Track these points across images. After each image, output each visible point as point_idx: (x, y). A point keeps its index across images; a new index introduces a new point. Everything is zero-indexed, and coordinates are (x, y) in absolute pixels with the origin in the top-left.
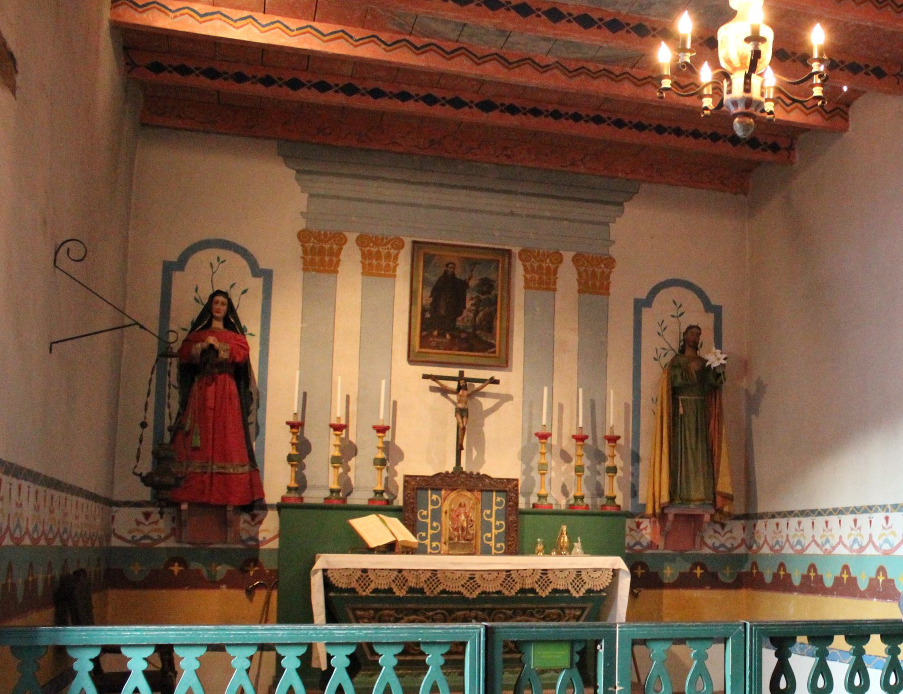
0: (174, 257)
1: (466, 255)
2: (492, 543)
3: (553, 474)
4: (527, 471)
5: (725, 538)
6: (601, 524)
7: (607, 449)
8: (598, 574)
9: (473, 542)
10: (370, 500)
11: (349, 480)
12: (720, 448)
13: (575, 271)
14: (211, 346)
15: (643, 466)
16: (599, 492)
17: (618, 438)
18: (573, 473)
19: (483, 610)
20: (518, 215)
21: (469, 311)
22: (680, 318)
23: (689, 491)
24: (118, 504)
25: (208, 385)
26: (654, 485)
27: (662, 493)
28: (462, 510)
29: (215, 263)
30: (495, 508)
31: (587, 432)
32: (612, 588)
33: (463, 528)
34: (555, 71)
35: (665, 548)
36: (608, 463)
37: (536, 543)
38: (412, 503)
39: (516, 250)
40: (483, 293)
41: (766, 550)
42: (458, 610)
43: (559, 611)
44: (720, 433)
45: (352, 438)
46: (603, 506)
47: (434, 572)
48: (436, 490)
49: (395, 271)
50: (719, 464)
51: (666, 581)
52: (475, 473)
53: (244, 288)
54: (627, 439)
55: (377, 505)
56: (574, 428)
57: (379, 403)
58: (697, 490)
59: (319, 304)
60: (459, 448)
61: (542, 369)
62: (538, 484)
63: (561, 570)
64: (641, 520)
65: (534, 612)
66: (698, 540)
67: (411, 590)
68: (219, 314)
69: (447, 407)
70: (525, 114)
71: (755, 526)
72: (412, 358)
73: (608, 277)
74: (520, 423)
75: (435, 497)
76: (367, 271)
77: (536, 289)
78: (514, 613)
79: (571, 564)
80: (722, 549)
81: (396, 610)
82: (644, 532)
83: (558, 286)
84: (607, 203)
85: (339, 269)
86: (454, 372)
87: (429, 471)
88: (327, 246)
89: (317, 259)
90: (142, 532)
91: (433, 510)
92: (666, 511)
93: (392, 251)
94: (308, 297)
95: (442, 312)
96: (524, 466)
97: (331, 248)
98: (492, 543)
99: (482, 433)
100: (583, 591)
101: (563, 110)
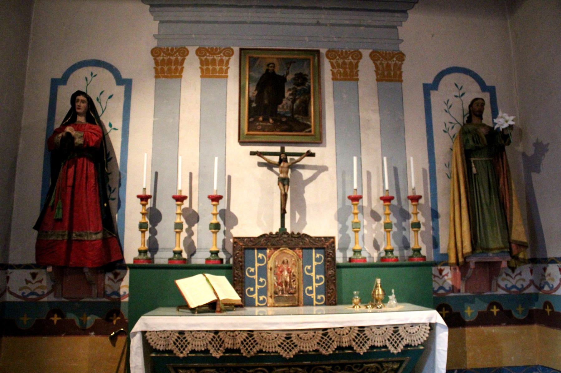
1: (282, 56)
2: (313, 296)
3: (366, 232)
4: (343, 230)
5: (515, 280)
6: (412, 277)
7: (410, 208)
8: (415, 329)
9: (296, 295)
10: (208, 260)
11: (193, 242)
12: (511, 201)
13: (373, 65)
14: (69, 134)
15: (441, 221)
16: (406, 246)
17: (420, 197)
18: (382, 230)
19: (302, 367)
20: (323, 25)
22: (462, 98)
24: (13, 267)
25: (69, 167)
26: (454, 235)
28: (285, 266)
29: (89, 78)
30: (315, 263)
31: (393, 194)
32: (429, 344)
33: (286, 282)
35: (466, 292)
36: (412, 220)
37: (353, 295)
38: (241, 262)
39: (323, 51)
40: (298, 85)
43: (377, 365)
44: (510, 189)
45: (195, 208)
46: (411, 258)
47: (250, 333)
48: (262, 249)
49: (226, 72)
50: (511, 215)
51: (467, 320)
52: (296, 233)
53: (111, 94)
55: (210, 264)
56: (381, 190)
58: (495, 240)
59: (167, 103)
60: (283, 212)
61: (351, 143)
63: (379, 327)
64: (442, 268)
67: (227, 350)
68: (86, 111)
71: (545, 269)
72: (241, 140)
73: (400, 68)
74: (335, 190)
75: (260, 255)
76: (205, 74)
80: (514, 290)
82: (446, 278)
84: (394, 11)
86: (277, 149)
87: (256, 232)
88: (173, 58)
89: (166, 68)
90: (29, 288)
91: (259, 268)
92: (467, 260)
93: (224, 58)
94: (158, 97)
95: (266, 102)
96: (340, 226)
97: (177, 59)
99: (303, 200)
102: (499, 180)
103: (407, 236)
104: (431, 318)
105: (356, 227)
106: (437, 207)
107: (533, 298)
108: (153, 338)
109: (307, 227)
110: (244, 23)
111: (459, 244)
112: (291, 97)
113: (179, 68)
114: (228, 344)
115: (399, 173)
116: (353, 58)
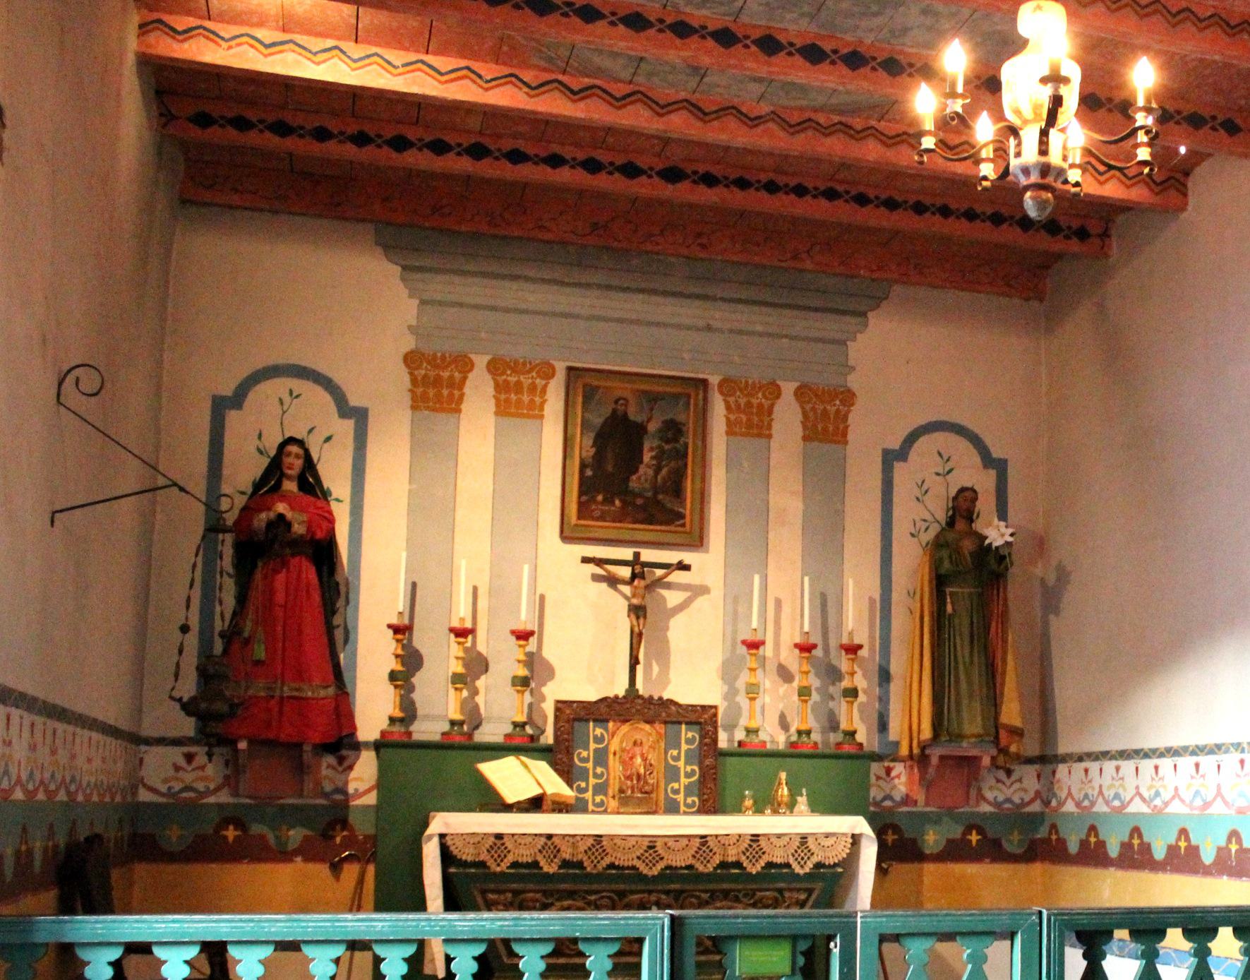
0: (227, 390)
2: (680, 797)
3: (767, 699)
4: (730, 695)
5: (1012, 790)
6: (836, 770)
7: (844, 664)
9: (654, 795)
10: (507, 736)
11: (477, 707)
12: (1004, 661)
13: (799, 410)
14: (281, 517)
15: (895, 687)
16: (833, 725)
18: (796, 697)
19: (667, 892)
21: (648, 466)
23: (960, 724)
24: (149, 742)
26: (911, 715)
27: (923, 726)
28: (637, 750)
29: (287, 399)
30: (684, 747)
31: (816, 638)
33: (639, 776)
34: (770, 125)
35: (927, 804)
36: (846, 683)
37: (743, 798)
38: (567, 740)
39: (714, 380)
40: (667, 442)
41: (1070, 807)
42: (632, 892)
43: (776, 894)
44: (1005, 641)
45: (482, 647)
46: (838, 745)
48: (601, 721)
49: (542, 409)
50: (1003, 684)
51: (927, 852)
54: (872, 650)
57: (519, 597)
58: (972, 722)
59: (435, 456)
60: (634, 662)
61: (752, 548)
62: (745, 714)
63: (779, 836)
64: (892, 764)
65: (740, 895)
66: (973, 793)
67: (566, 864)
69: (616, 604)
70: (727, 186)
71: (1054, 772)
72: (566, 533)
73: (845, 418)
75: (599, 731)
76: (503, 409)
77: (742, 435)
78: (711, 897)
79: (795, 827)
80: (1007, 805)
81: (544, 893)
82: (896, 781)
83: (774, 432)
85: (463, 407)
86: (626, 553)
87: (591, 695)
88: (446, 374)
89: (431, 392)
90: (183, 781)
91: (596, 750)
92: (927, 752)
94: (418, 447)
95: (610, 468)
97: (451, 377)
98: (680, 797)
100: (810, 865)
101: (781, 180)
102: (990, 624)
103: (837, 712)
104: (854, 827)
105: (753, 691)
106: (888, 662)
107: (1035, 820)
108: (458, 843)
109: (670, 688)
110: (578, 317)
111: (915, 727)
112: (654, 462)
113: (456, 393)
114: (566, 854)
115: (829, 604)
116: (764, 396)
